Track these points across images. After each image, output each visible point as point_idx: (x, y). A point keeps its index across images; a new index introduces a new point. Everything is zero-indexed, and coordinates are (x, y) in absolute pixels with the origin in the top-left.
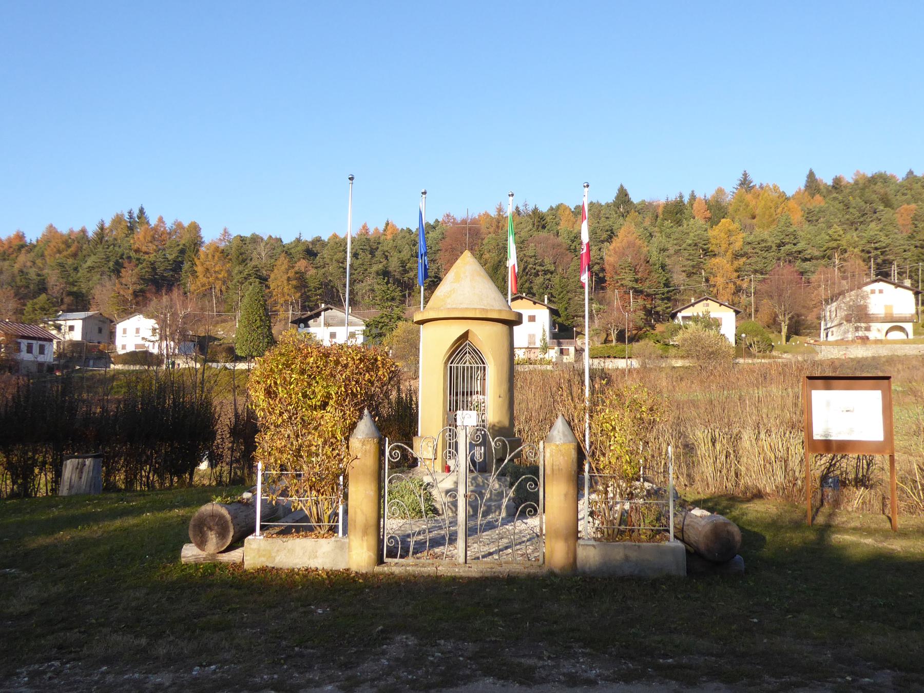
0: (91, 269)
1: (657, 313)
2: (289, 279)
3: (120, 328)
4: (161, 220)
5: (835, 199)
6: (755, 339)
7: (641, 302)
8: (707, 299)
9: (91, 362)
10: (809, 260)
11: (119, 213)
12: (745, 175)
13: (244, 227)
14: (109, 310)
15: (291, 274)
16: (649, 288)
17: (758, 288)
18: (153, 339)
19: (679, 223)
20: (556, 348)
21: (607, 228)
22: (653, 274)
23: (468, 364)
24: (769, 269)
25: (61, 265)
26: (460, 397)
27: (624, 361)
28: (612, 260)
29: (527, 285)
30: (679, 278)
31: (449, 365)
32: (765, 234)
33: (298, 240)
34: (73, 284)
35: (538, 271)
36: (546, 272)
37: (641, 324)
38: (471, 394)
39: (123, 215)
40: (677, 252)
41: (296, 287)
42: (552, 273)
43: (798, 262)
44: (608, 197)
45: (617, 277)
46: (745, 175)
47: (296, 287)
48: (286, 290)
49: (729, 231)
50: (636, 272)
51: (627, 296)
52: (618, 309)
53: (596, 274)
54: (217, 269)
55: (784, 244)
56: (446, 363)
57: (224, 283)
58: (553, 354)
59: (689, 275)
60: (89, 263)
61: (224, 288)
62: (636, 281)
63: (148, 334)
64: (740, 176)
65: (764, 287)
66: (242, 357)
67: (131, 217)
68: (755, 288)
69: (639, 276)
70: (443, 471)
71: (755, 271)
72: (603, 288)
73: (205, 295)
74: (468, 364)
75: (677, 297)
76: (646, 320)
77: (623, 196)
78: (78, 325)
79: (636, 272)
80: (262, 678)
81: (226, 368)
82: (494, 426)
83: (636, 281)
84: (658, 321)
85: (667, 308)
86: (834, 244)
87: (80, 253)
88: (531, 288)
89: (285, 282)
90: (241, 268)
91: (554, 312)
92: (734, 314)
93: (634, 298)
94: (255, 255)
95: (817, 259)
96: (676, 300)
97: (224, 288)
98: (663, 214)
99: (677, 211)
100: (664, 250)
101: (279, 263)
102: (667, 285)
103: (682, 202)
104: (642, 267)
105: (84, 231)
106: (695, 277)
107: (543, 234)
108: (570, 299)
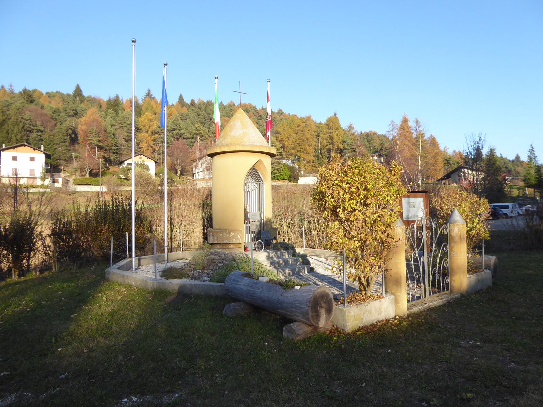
5: (193, 110)
7: (102, 153)
8: (141, 155)
10: (186, 139)
12: (149, 91)
16: (106, 146)
20: (49, 178)
21: (73, 108)
22: (109, 138)
27: (99, 187)
29: (25, 138)
35: (33, 129)
36: (38, 131)
42: (42, 131)
43: (181, 140)
44: (70, 90)
46: (78, 85)
51: (93, 150)
55: (174, 129)
58: (47, 182)
62: (100, 141)
64: (147, 91)
69: (101, 139)
75: (121, 152)
77: (78, 91)
80: (131, 400)
83: (100, 141)
84: (110, 165)
85: (117, 158)
86: (198, 132)
88: (28, 140)
91: (48, 156)
95: (189, 138)
96: (121, 154)
99: (115, 104)
107: (32, 106)
108: (55, 149)
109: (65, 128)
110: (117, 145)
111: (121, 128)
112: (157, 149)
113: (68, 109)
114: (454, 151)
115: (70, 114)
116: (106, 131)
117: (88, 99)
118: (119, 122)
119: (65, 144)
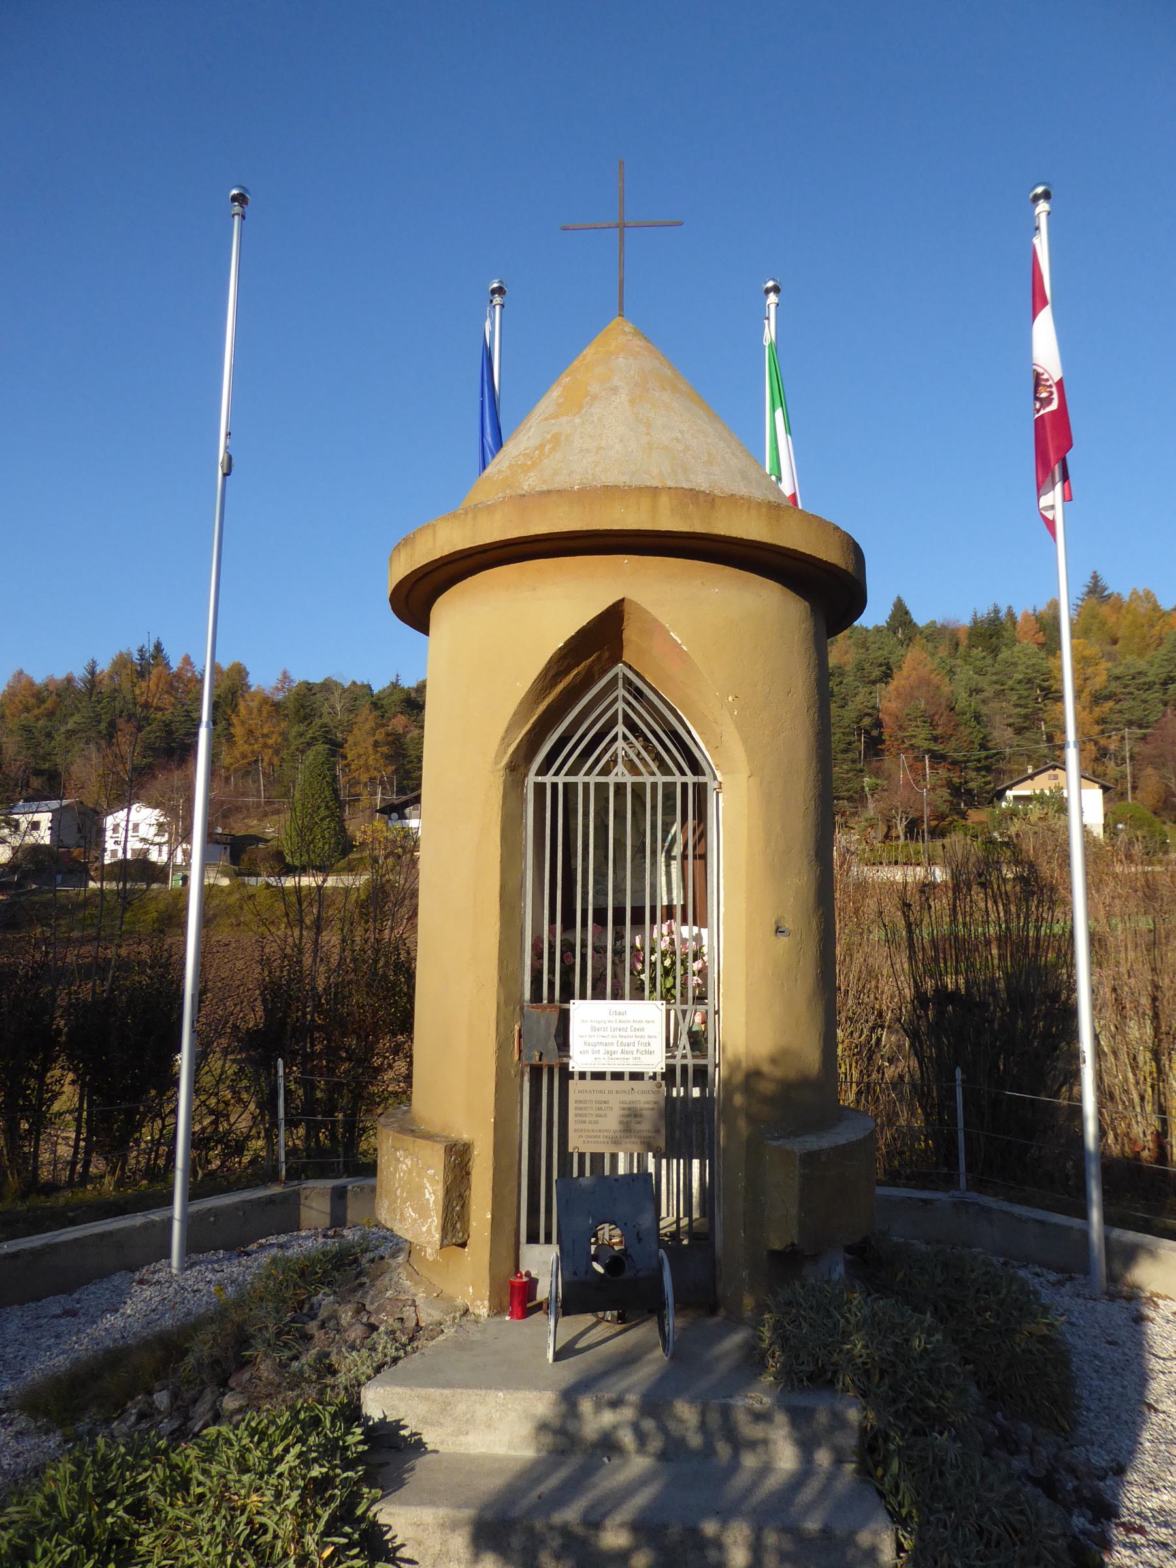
0: (70, 734)
1: (969, 792)
2: (376, 744)
3: (110, 821)
4: (187, 660)
6: (1138, 833)
9: (59, 877)
11: (124, 651)
13: (311, 670)
14: (92, 795)
15: (380, 736)
16: (955, 750)
17: (1136, 750)
18: (157, 839)
19: (994, 651)
21: (881, 660)
23: (620, 774)
24: (1152, 718)
25: (27, 729)
26: (585, 934)
28: (893, 706)
30: (1002, 735)
31: (532, 779)
32: (1142, 665)
33: (395, 685)
34: (44, 758)
37: (945, 808)
38: (638, 919)
39: (129, 654)
40: (999, 694)
41: (387, 757)
45: (901, 734)
46: (1095, 578)
47: (387, 757)
48: (371, 762)
49: (1084, 658)
50: (933, 725)
52: (907, 784)
53: (867, 732)
54: (266, 731)
56: (516, 767)
57: (277, 752)
59: (1019, 731)
60: (70, 726)
61: (276, 761)
62: (935, 739)
63: (148, 832)
64: (1087, 580)
65: (1147, 749)
66: (296, 868)
67: (142, 658)
68: (1131, 750)
70: (497, 1309)
71: (1130, 724)
72: (878, 753)
73: (247, 773)
74: (620, 774)
75: (1001, 765)
76: (951, 802)
78: (45, 819)
79: (933, 725)
81: (268, 886)
82: (754, 1074)
83: (935, 739)
84: (970, 805)
87: (58, 712)
89: (370, 749)
90: (302, 728)
92: (1101, 791)
93: (931, 768)
94: (325, 709)
96: (1000, 772)
97: (276, 761)
98: (969, 638)
100: (978, 691)
101: (360, 719)
102: (983, 747)
103: (998, 619)
104: (943, 718)
105: (69, 680)
106: (1028, 734)
109: (853, 715)
110: (990, 745)
111: (999, 694)
112: (1112, 747)
113: (867, 666)
114: (354, 683)
115: (873, 678)
116: (952, 709)
117: (928, 631)
118: (994, 678)
119: (850, 755)
